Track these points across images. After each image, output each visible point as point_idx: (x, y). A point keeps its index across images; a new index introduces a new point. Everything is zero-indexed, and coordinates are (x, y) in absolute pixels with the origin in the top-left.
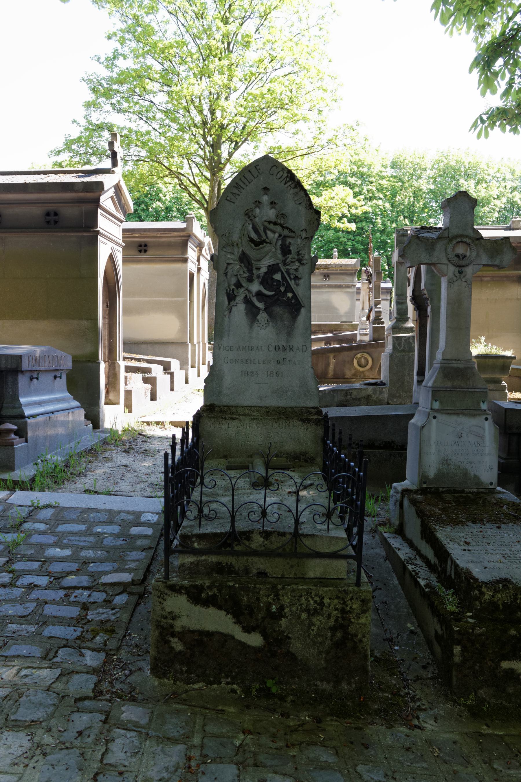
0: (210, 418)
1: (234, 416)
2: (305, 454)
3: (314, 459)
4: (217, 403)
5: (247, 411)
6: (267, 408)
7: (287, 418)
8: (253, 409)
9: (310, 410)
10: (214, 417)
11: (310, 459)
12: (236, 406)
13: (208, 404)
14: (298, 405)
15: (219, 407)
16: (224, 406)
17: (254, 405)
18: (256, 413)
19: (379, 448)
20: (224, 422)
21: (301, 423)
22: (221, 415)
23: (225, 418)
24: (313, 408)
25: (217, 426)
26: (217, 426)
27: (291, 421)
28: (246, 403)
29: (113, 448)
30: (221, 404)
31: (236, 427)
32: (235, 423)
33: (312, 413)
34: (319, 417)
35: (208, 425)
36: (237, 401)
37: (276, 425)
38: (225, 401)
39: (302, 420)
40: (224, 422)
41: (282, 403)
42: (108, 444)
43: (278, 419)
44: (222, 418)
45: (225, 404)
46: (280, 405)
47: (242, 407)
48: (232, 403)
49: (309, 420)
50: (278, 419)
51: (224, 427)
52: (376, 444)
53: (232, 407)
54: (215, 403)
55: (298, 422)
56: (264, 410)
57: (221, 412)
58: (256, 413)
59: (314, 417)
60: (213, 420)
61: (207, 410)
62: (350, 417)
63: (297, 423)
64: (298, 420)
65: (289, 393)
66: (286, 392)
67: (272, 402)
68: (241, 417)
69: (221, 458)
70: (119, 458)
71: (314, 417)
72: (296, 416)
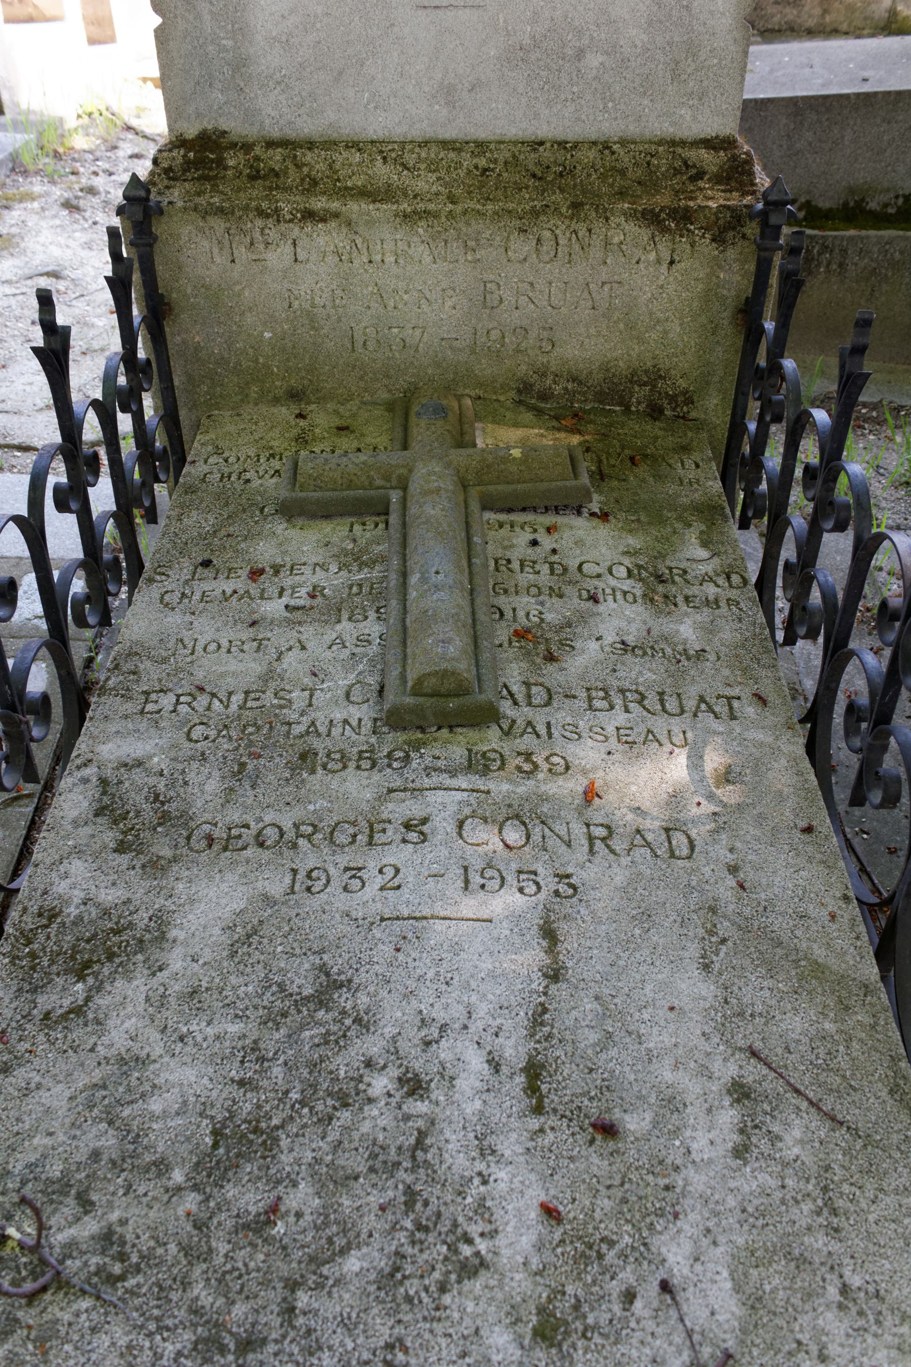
0: (206, 213)
1: (319, 204)
2: (654, 377)
3: (689, 401)
4: (235, 125)
5: (382, 172)
6: (481, 146)
7: (576, 206)
8: (410, 159)
9: (692, 155)
10: (221, 211)
11: (673, 399)
12: (330, 144)
13: (191, 132)
14: (633, 130)
15: (247, 147)
16: (271, 144)
17: (417, 132)
18: (425, 183)
19: (881, 219)
20: (273, 234)
21: (645, 234)
22: (257, 191)
23: (276, 215)
24: (709, 144)
25: (241, 252)
26: (241, 252)
27: (599, 226)
28: (378, 125)
29: (37, 189)
30: (250, 132)
31: (331, 259)
32: (323, 239)
33: (700, 175)
34: (734, 200)
35: (199, 252)
36: (331, 115)
37: (522, 247)
38: (273, 112)
39: (651, 218)
40: (273, 234)
41: (554, 121)
42: (25, 173)
43: (535, 213)
44: (261, 213)
45: (276, 134)
46: (545, 130)
47: (354, 145)
48: (307, 126)
49: (684, 217)
50: (535, 213)
51: (278, 257)
52: (873, 205)
53: (311, 145)
54: (224, 125)
55: (631, 227)
56: (467, 161)
57: (254, 177)
58: (425, 183)
59: (714, 199)
60: (219, 224)
61: (188, 165)
62: (793, 102)
63: (627, 232)
64: (631, 215)
65: (594, 60)
66: (580, 54)
67: (508, 114)
68: (354, 208)
69: (276, 401)
70: (46, 236)
71: (714, 199)
72: (622, 194)
